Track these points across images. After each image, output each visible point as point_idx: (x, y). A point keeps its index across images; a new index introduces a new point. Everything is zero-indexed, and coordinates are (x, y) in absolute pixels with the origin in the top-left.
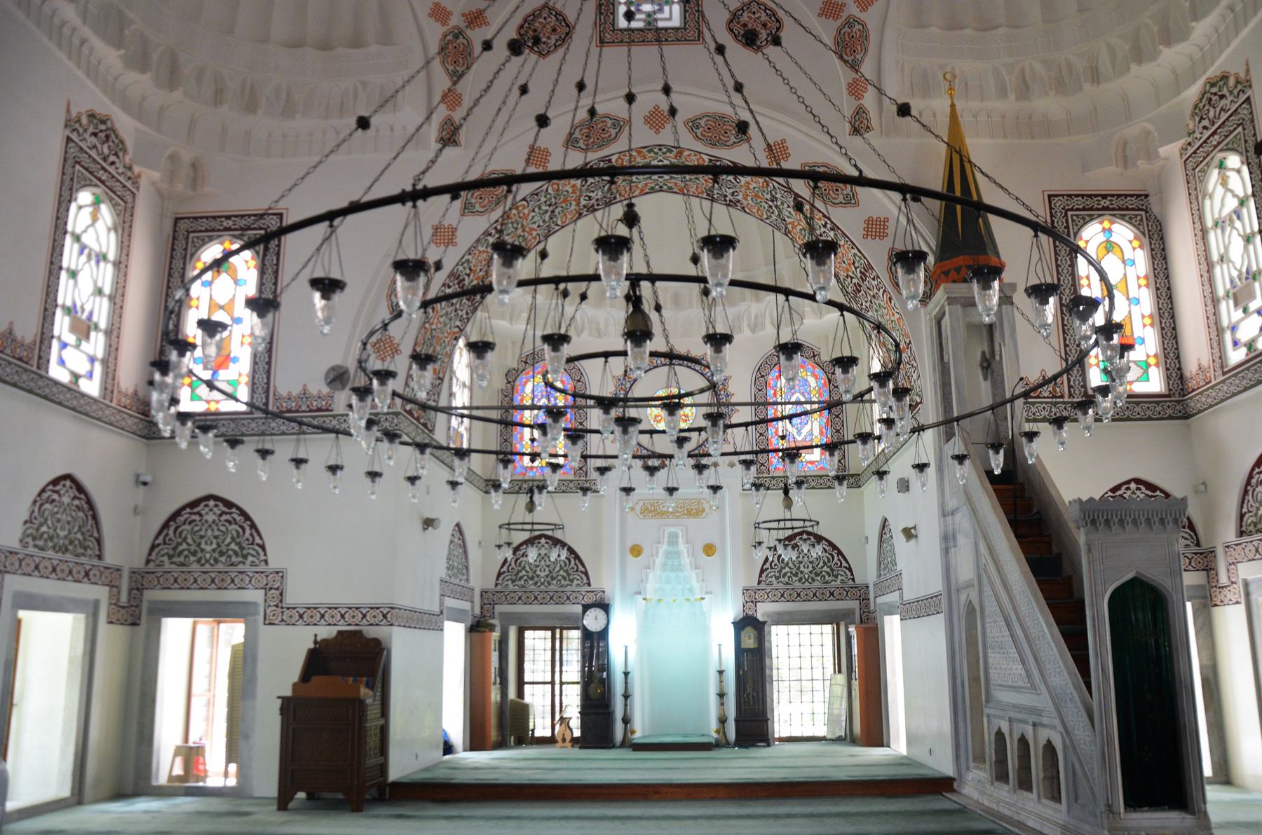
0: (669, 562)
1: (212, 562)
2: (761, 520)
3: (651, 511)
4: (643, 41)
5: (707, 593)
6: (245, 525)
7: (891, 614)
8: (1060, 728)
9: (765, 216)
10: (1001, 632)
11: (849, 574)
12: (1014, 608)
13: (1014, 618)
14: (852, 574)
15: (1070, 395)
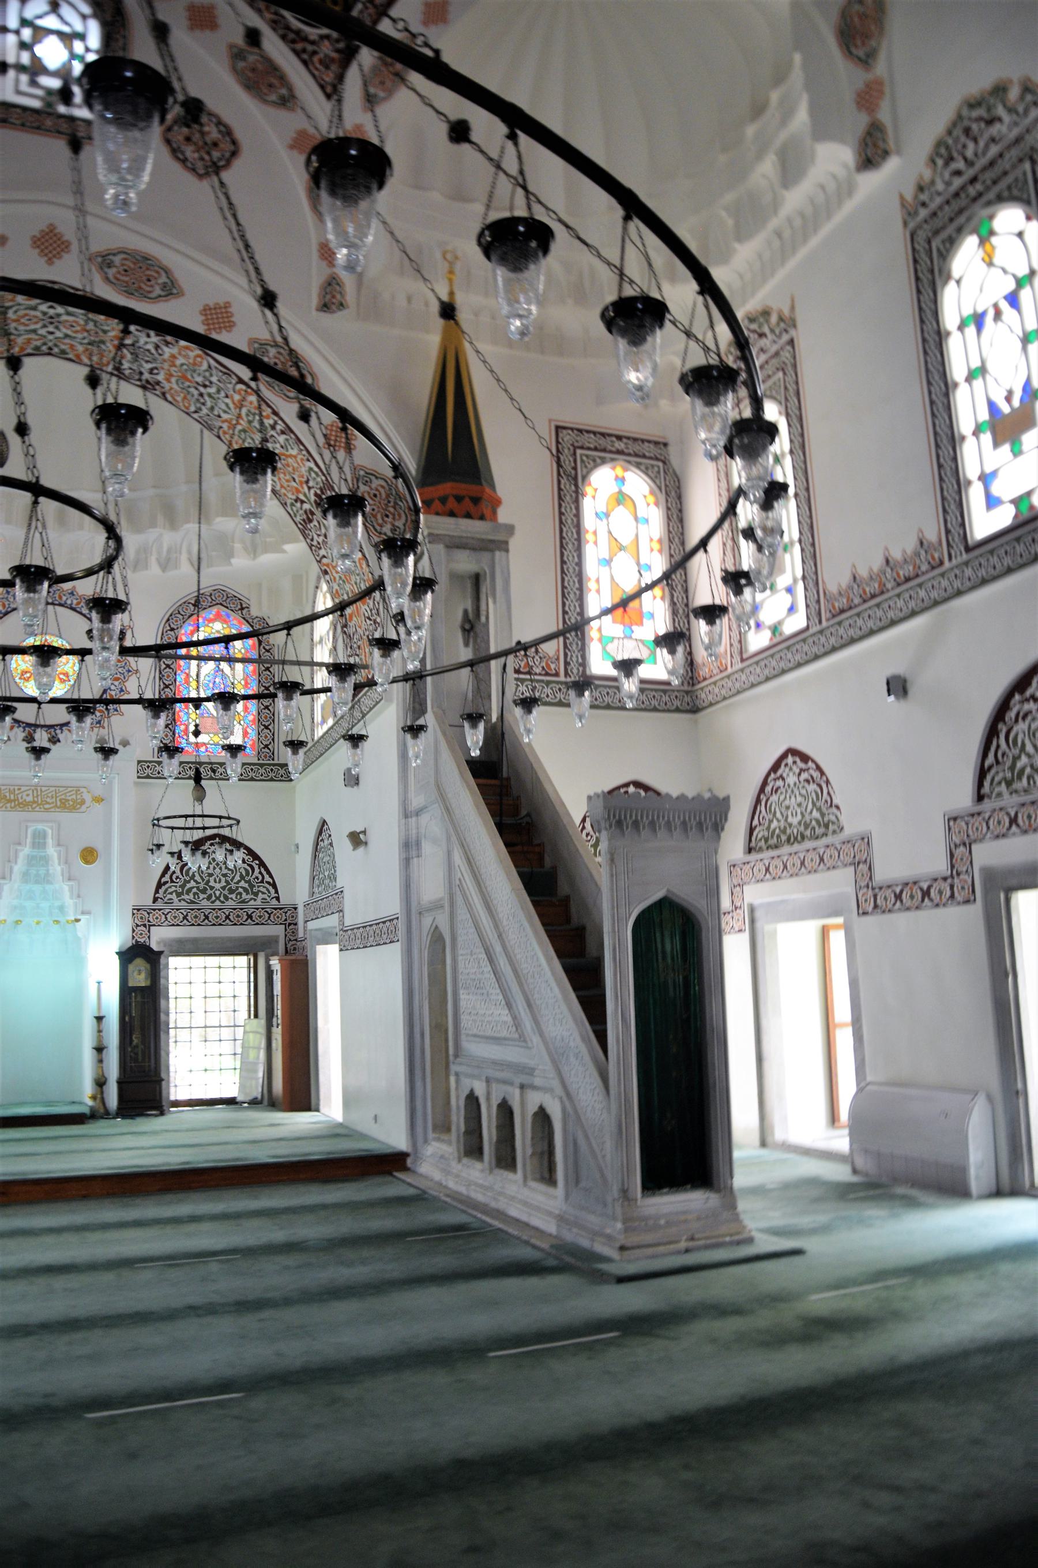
0: (33, 871)
1: (222, 899)
2: (161, 815)
3: (10, 801)
4: (38, 128)
5: (83, 913)
6: (253, 864)
7: (327, 943)
8: (559, 1091)
9: (193, 409)
10: (480, 967)
11: (272, 891)
12: (500, 936)
13: (498, 948)
14: (277, 892)
15: (566, 674)
